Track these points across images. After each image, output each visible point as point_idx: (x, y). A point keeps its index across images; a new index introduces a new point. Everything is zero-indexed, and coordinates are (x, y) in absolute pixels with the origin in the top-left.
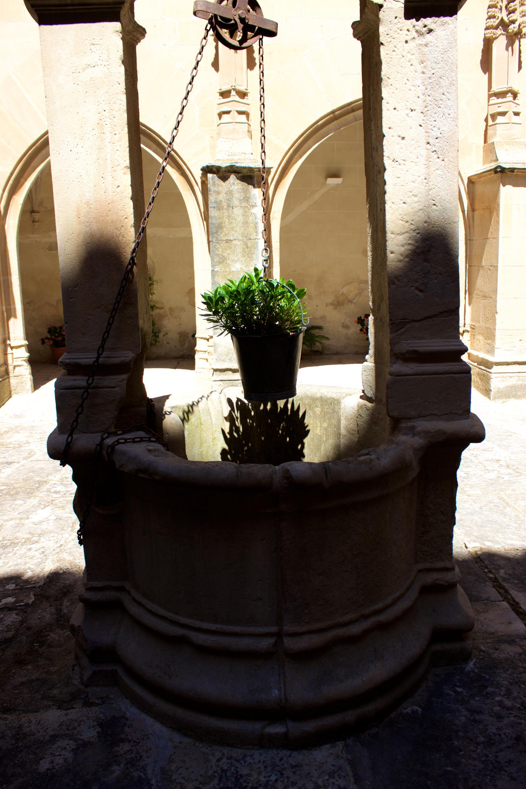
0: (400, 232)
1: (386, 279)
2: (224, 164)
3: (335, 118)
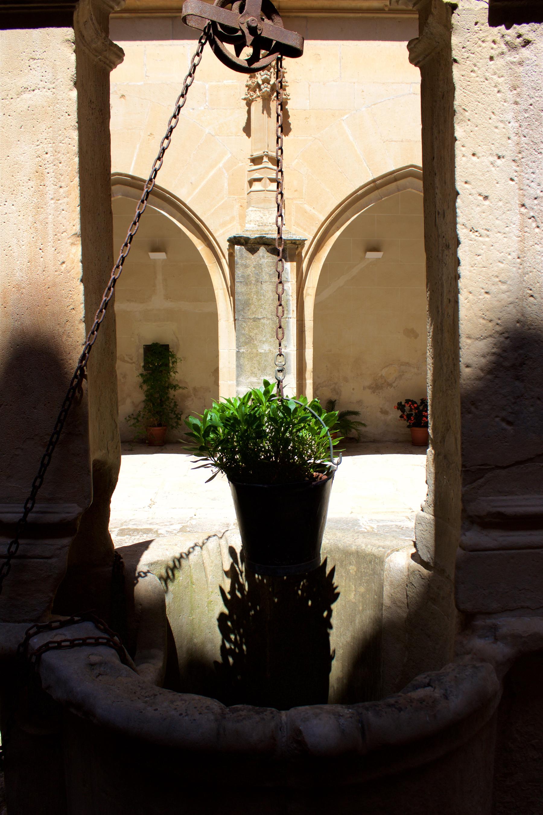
0: (480, 336)
1: (457, 402)
2: (253, 236)
3: (377, 188)
